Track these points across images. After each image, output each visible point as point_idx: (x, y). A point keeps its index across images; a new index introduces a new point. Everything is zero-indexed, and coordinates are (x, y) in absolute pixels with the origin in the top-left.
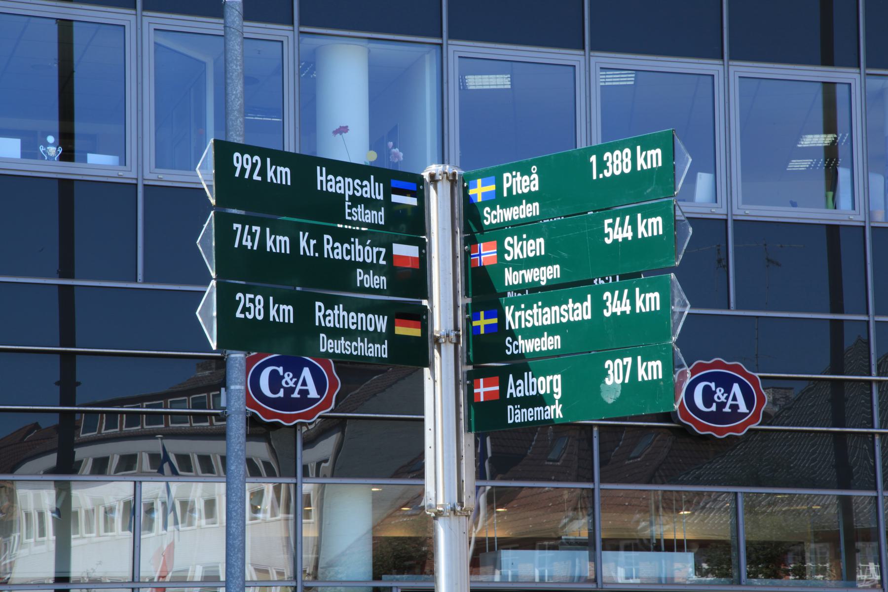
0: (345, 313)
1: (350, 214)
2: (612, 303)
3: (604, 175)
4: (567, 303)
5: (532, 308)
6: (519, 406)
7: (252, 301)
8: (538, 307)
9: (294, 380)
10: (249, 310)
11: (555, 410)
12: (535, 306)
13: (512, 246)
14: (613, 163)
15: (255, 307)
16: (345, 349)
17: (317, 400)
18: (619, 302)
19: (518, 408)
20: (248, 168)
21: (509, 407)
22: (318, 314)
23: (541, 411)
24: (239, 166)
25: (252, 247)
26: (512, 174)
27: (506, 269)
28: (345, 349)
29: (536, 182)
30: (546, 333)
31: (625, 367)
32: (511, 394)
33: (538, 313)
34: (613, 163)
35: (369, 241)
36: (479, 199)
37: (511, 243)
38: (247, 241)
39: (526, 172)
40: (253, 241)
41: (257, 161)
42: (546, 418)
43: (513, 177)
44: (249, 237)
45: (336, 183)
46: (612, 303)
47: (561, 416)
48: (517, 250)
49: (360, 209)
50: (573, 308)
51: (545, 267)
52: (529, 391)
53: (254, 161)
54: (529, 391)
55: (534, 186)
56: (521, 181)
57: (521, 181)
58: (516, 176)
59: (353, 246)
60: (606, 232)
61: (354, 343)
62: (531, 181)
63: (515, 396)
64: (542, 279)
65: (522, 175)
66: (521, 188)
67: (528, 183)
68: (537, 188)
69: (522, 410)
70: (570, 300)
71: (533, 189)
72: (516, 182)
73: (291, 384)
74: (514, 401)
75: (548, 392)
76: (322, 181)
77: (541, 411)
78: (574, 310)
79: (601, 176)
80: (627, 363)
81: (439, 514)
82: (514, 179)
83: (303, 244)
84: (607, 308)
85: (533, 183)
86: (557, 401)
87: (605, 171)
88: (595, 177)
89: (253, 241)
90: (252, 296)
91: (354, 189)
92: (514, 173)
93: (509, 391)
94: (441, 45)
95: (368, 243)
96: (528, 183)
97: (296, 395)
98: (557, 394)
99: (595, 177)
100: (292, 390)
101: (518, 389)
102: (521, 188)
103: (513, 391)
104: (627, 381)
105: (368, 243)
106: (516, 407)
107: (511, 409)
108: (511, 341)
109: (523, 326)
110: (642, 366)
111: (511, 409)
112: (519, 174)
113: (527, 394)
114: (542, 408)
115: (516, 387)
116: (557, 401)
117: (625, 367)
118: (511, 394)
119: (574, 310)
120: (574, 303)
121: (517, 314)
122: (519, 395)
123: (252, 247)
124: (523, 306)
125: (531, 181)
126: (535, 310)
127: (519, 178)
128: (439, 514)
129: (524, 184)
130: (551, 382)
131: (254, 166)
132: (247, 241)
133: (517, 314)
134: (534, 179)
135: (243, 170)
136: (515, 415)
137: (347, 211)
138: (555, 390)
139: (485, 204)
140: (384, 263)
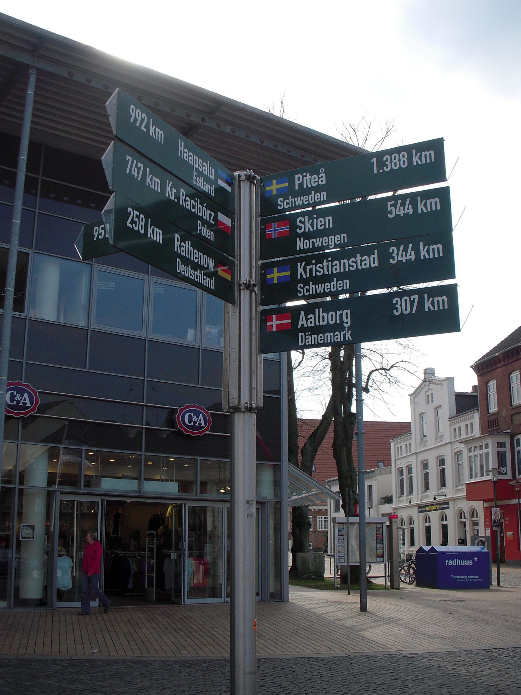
0: (192, 248)
1: (196, 181)
2: (397, 254)
3: (383, 170)
4: (355, 257)
5: (322, 263)
6: (310, 333)
7: (137, 217)
8: (328, 261)
9: (21, 398)
10: (135, 223)
11: (344, 335)
12: (325, 261)
13: (304, 223)
14: (391, 162)
15: (139, 222)
16: (191, 275)
17: (31, 407)
18: (404, 253)
19: (308, 335)
20: (139, 119)
21: (300, 334)
22: (176, 243)
23: (331, 336)
24: (133, 115)
25: (138, 177)
26: (302, 175)
27: (298, 239)
28: (191, 275)
29: (324, 178)
30: (335, 279)
31: (412, 303)
32: (302, 325)
33: (328, 266)
34: (391, 162)
35: (205, 204)
36: (274, 193)
37: (303, 220)
38: (134, 171)
39: (315, 172)
40: (138, 173)
41: (144, 117)
42: (336, 340)
43: (303, 177)
44: (136, 169)
45: (189, 156)
46: (397, 254)
47: (351, 339)
48: (308, 226)
49: (202, 180)
50: (361, 260)
51: (333, 236)
52: (319, 322)
53: (143, 117)
54: (319, 322)
55: (322, 181)
56: (310, 179)
57: (310, 179)
58: (306, 176)
59: (196, 203)
60: (389, 209)
61: (196, 272)
62: (319, 178)
63: (306, 326)
64: (330, 244)
65: (311, 175)
66: (310, 183)
67: (317, 180)
68: (324, 182)
69: (313, 336)
70: (358, 255)
71: (321, 183)
72: (306, 179)
73: (19, 399)
74: (304, 329)
75: (338, 322)
76: (181, 151)
77: (331, 336)
78: (361, 261)
79: (381, 171)
80: (414, 299)
81: (236, 409)
82: (305, 178)
83: (168, 189)
84: (393, 258)
85: (321, 180)
86: (346, 329)
87: (385, 168)
88: (375, 172)
89: (138, 173)
90: (138, 214)
91: (199, 165)
92: (305, 174)
93: (300, 323)
94: (92, 264)
95: (205, 205)
96: (317, 180)
97: (21, 404)
98: (347, 323)
99: (375, 172)
100: (19, 402)
101: (309, 321)
102: (310, 183)
103: (304, 322)
104: (414, 311)
105: (205, 205)
106: (307, 334)
107: (302, 336)
108: (302, 286)
109: (314, 275)
110: (348, 333)
111: (302, 336)
112: (308, 174)
113: (318, 324)
114: (332, 334)
115: (307, 320)
116: (346, 329)
117: (412, 303)
118: (302, 325)
119: (361, 261)
120: (361, 256)
121: (308, 268)
122: (310, 325)
123: (138, 177)
124: (314, 262)
125: (319, 178)
126: (325, 263)
127: (309, 177)
128: (236, 409)
129: (313, 181)
130: (341, 315)
131: (143, 120)
132: (134, 171)
133: (308, 268)
134: (322, 177)
135: (136, 120)
136: (305, 339)
137: (194, 178)
138: (345, 320)
139: (278, 196)
140: (213, 223)
